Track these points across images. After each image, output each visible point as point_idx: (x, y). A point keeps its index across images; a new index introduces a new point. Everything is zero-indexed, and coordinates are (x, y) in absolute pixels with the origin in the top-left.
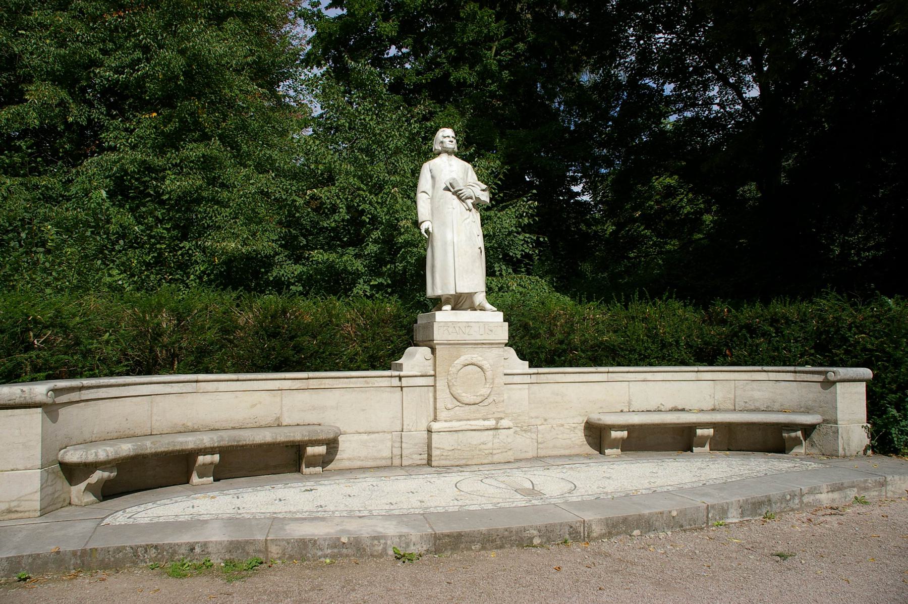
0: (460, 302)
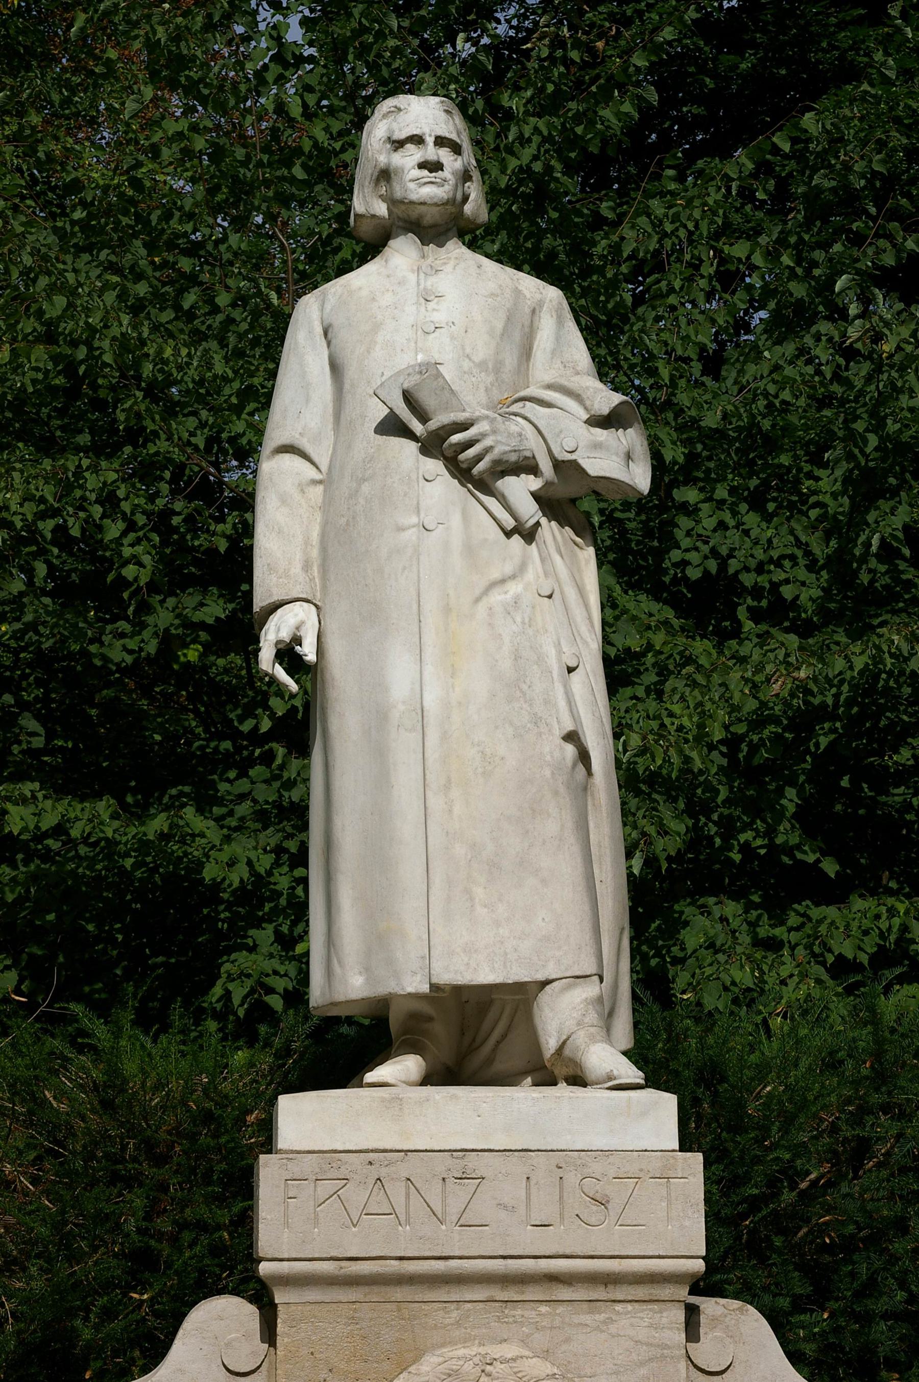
0: (475, 1036)
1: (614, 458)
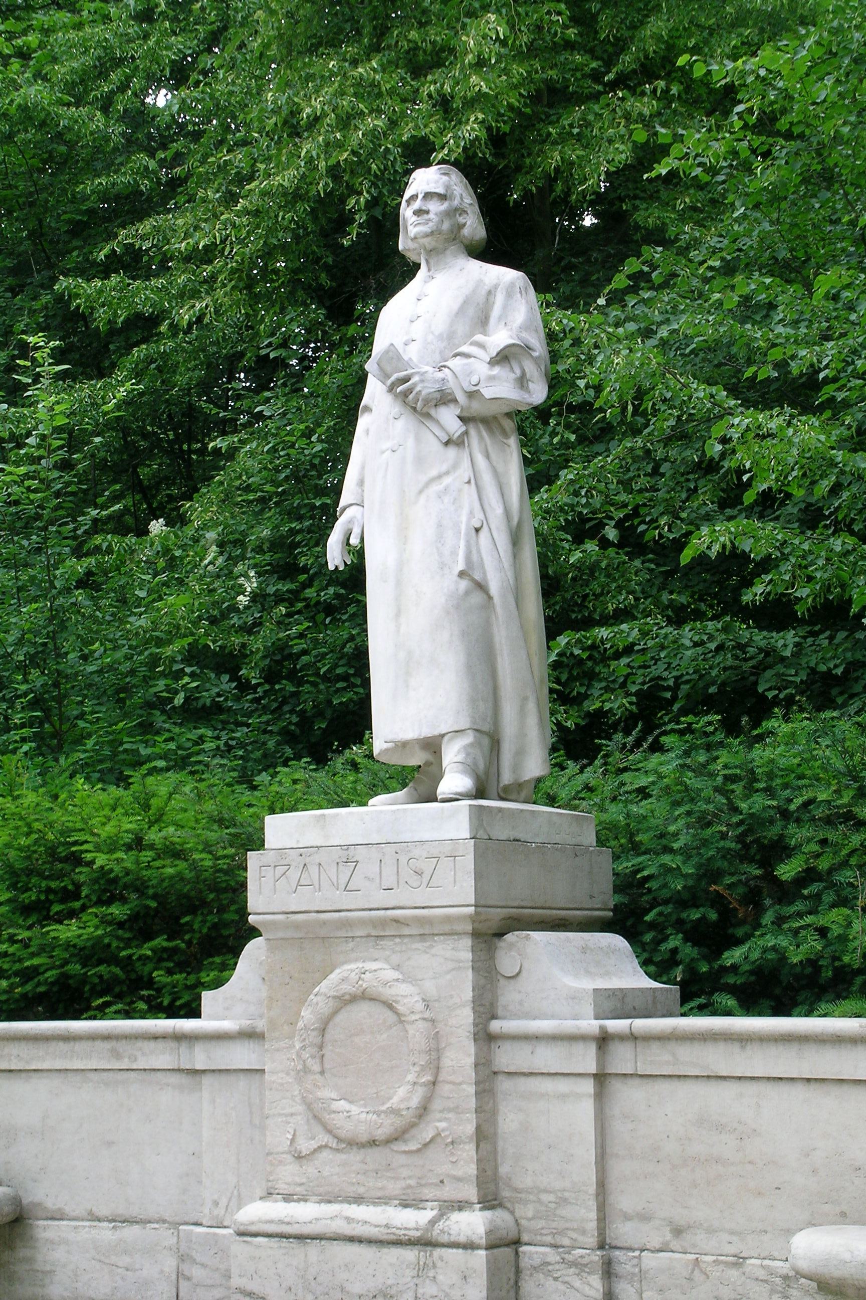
1: (505, 384)
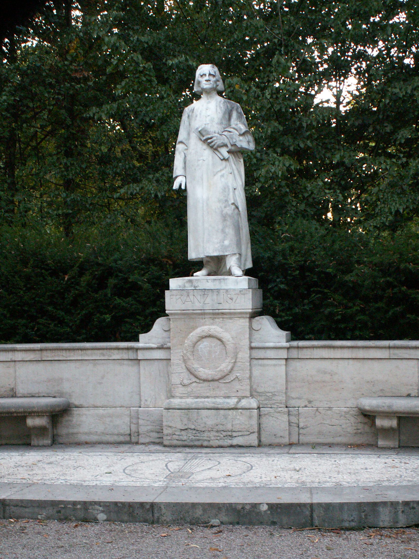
0: (216, 266)
